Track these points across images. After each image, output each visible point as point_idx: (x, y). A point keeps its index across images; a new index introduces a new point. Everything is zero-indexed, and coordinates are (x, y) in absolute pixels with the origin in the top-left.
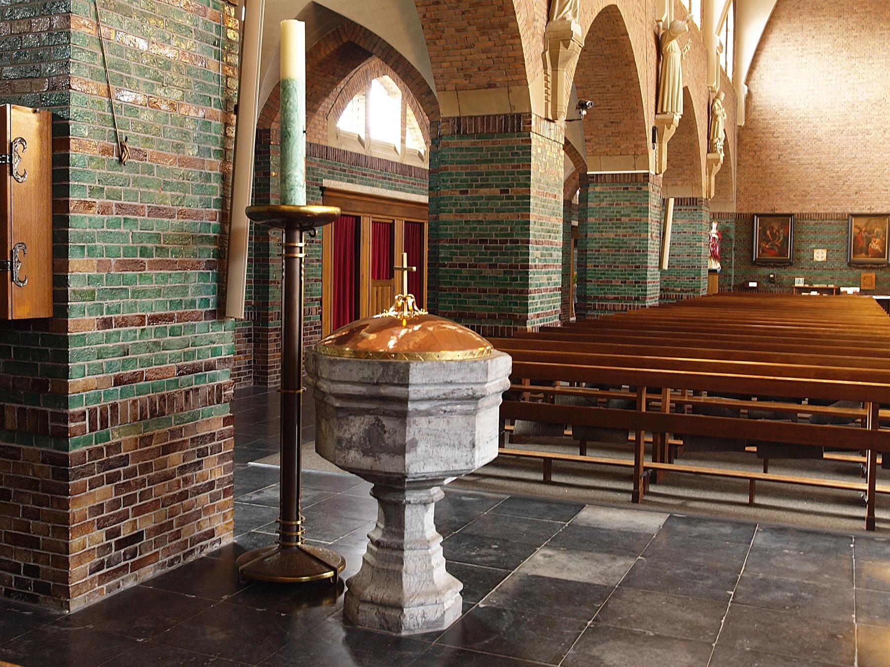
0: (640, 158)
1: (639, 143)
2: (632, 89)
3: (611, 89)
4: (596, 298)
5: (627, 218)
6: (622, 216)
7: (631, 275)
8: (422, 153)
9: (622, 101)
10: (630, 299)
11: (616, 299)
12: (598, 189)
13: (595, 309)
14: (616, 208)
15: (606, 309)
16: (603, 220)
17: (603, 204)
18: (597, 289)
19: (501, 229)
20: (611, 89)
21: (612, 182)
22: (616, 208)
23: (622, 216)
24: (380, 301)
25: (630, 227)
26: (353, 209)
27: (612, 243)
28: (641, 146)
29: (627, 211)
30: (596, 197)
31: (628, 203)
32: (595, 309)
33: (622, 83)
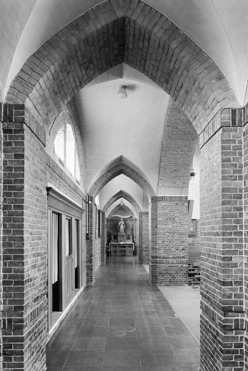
0: (185, 189)
1: (186, 181)
2: (191, 153)
3: (180, 152)
4: (164, 257)
5: (178, 218)
6: (175, 217)
7: (180, 246)
8: (79, 180)
9: (183, 160)
10: (180, 257)
11: (173, 258)
12: (163, 204)
13: (163, 263)
14: (172, 214)
15: (169, 263)
16: (166, 219)
17: (166, 211)
18: (164, 253)
19: (173, 276)
20: (180, 152)
21: (170, 201)
22: (172, 214)
23: (175, 217)
24: (68, 270)
25: (180, 223)
26: (59, 208)
27: (171, 230)
28: (186, 183)
29: (178, 215)
30: (162, 208)
31: (178, 211)
32: (163, 263)
33: (186, 149)
